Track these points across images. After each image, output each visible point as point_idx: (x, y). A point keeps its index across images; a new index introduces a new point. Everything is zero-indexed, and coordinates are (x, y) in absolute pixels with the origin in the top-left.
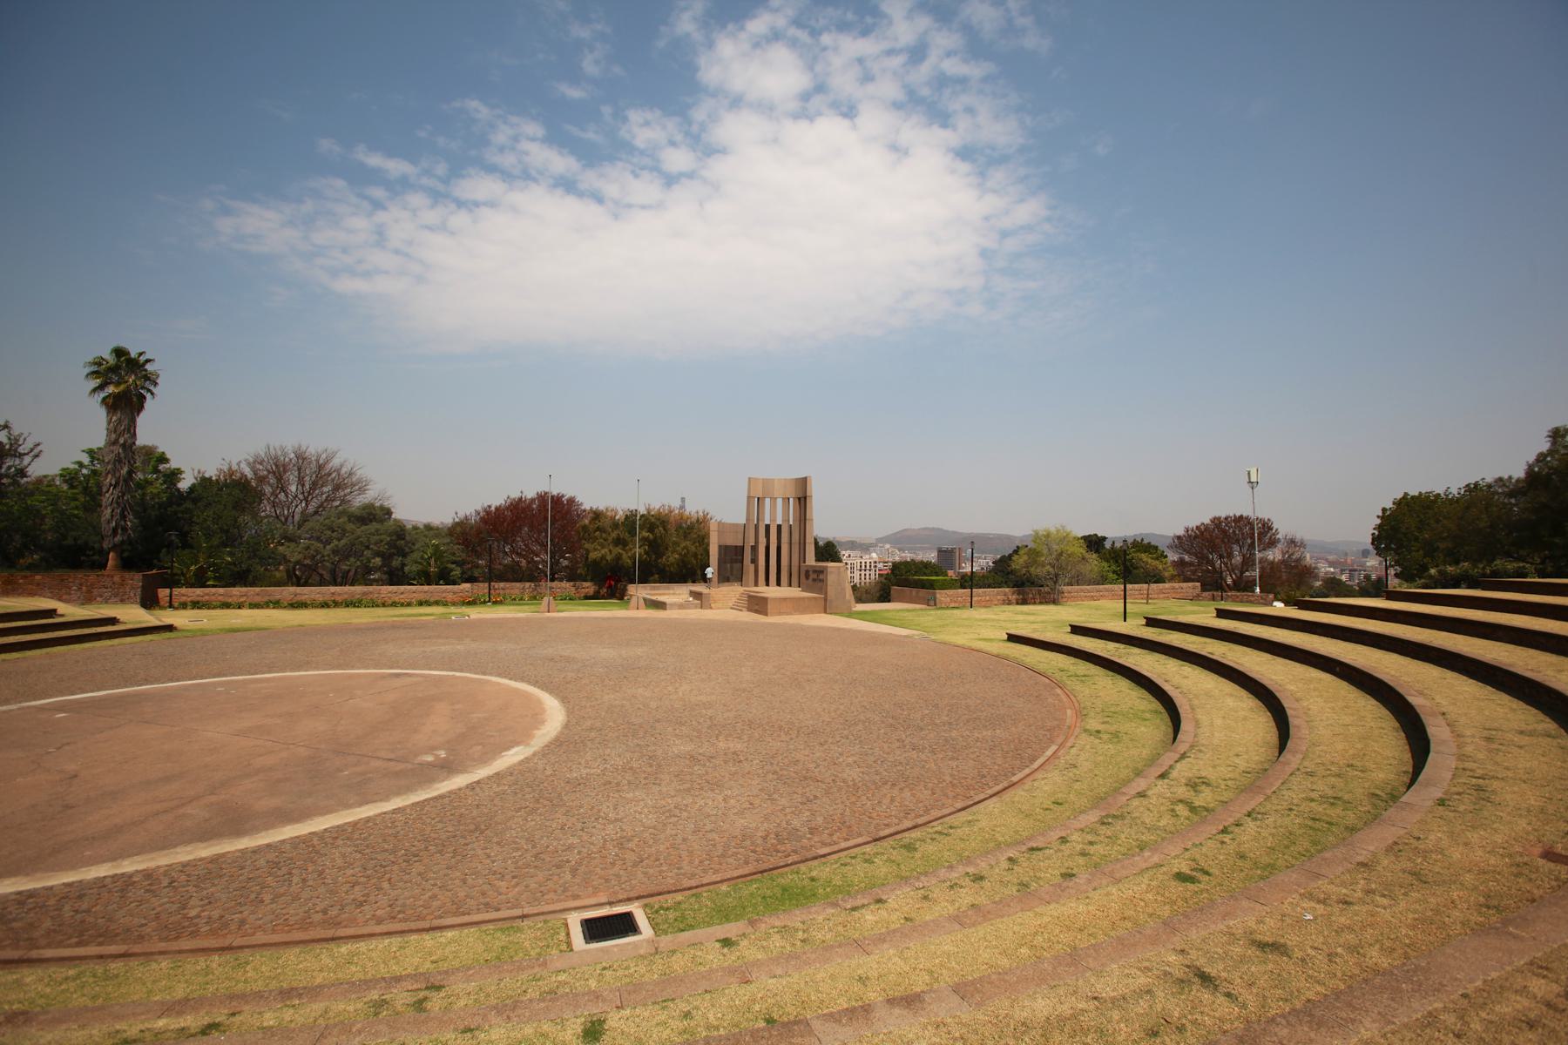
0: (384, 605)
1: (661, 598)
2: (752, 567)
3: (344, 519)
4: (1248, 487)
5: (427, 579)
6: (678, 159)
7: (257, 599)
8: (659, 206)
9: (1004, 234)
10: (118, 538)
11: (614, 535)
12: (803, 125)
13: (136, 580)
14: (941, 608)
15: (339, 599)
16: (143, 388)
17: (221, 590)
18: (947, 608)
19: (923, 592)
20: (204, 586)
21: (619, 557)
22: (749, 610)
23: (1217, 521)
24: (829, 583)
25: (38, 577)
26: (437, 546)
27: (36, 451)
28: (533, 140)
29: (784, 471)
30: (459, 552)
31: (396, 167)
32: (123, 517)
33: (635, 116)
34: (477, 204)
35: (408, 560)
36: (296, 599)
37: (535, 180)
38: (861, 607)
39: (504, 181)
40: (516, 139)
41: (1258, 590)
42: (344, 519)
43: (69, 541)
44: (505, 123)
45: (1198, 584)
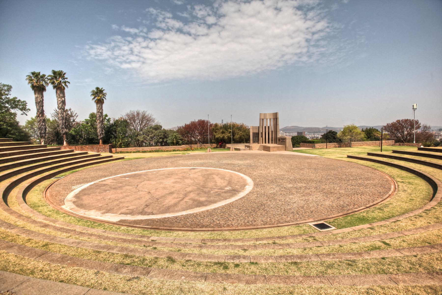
0: (165, 151)
1: (238, 148)
2: (261, 138)
3: (152, 129)
4: (412, 110)
5: (173, 144)
6: (211, 20)
7: (134, 151)
8: (207, 35)
9: (313, 34)
10: (102, 136)
11: (221, 131)
12: (247, 4)
13: (107, 146)
14: (317, 149)
15: (153, 150)
16: (103, 97)
17: (126, 149)
18: (318, 149)
19: (310, 144)
20: (121, 147)
21: (224, 137)
22: (264, 150)
23: (398, 121)
24: (287, 142)
25: (87, 146)
26: (175, 135)
27: (76, 115)
28: (169, 18)
29: (270, 111)
30: (179, 136)
31: (133, 31)
32: (102, 131)
33: (197, 8)
34: (156, 39)
35: (168, 139)
36: (143, 150)
37: (171, 30)
38: (294, 149)
39: (163, 31)
40: (164, 19)
41: (415, 142)
42: (152, 129)
43: (90, 137)
44: (161, 14)
45: (394, 141)
